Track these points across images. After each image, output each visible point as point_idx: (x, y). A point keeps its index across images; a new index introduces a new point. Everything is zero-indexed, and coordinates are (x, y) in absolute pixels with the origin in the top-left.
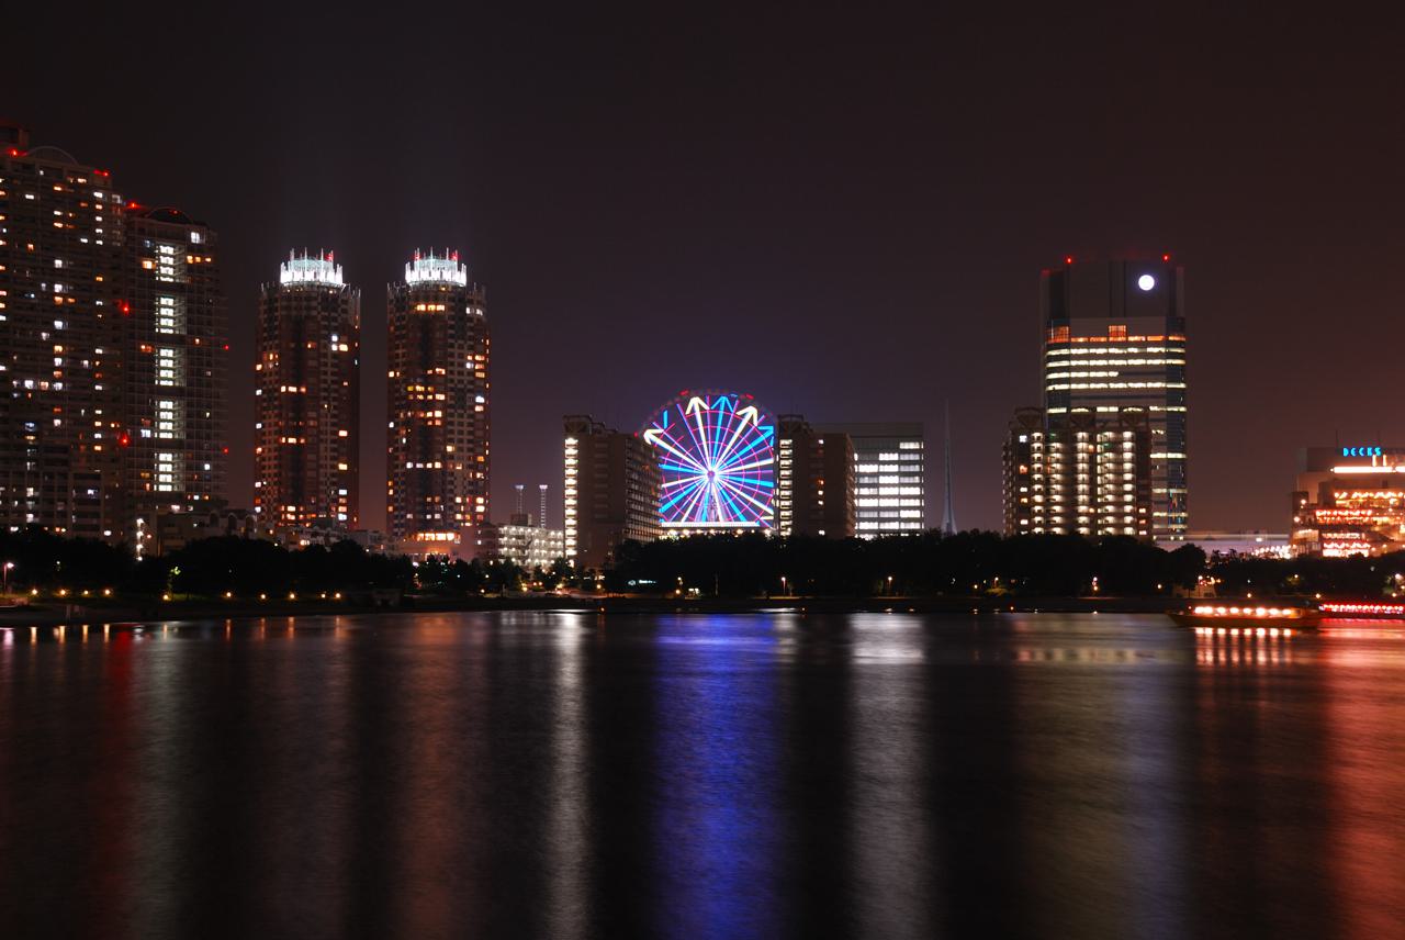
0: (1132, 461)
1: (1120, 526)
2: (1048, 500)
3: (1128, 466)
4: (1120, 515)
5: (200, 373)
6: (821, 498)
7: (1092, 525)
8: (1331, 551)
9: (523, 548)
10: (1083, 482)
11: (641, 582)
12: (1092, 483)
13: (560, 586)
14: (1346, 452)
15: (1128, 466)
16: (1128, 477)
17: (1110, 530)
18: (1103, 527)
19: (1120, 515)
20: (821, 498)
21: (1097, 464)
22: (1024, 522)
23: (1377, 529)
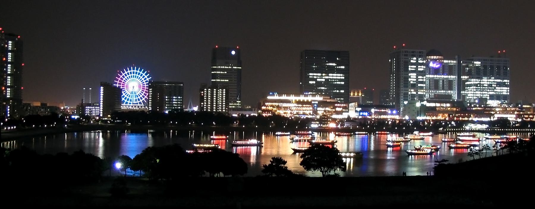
0: (225, 93)
1: (222, 109)
2: (207, 104)
3: (224, 103)
4: (222, 107)
5: (6, 84)
6: (158, 109)
7: (216, 109)
8: (264, 115)
9: (90, 112)
10: (215, 98)
11: (118, 121)
12: (217, 96)
13: (100, 122)
14: (270, 93)
15: (224, 97)
16: (224, 106)
17: (220, 110)
18: (219, 110)
19: (222, 107)
20: (158, 109)
21: (218, 98)
22: (202, 104)
23: (273, 111)
